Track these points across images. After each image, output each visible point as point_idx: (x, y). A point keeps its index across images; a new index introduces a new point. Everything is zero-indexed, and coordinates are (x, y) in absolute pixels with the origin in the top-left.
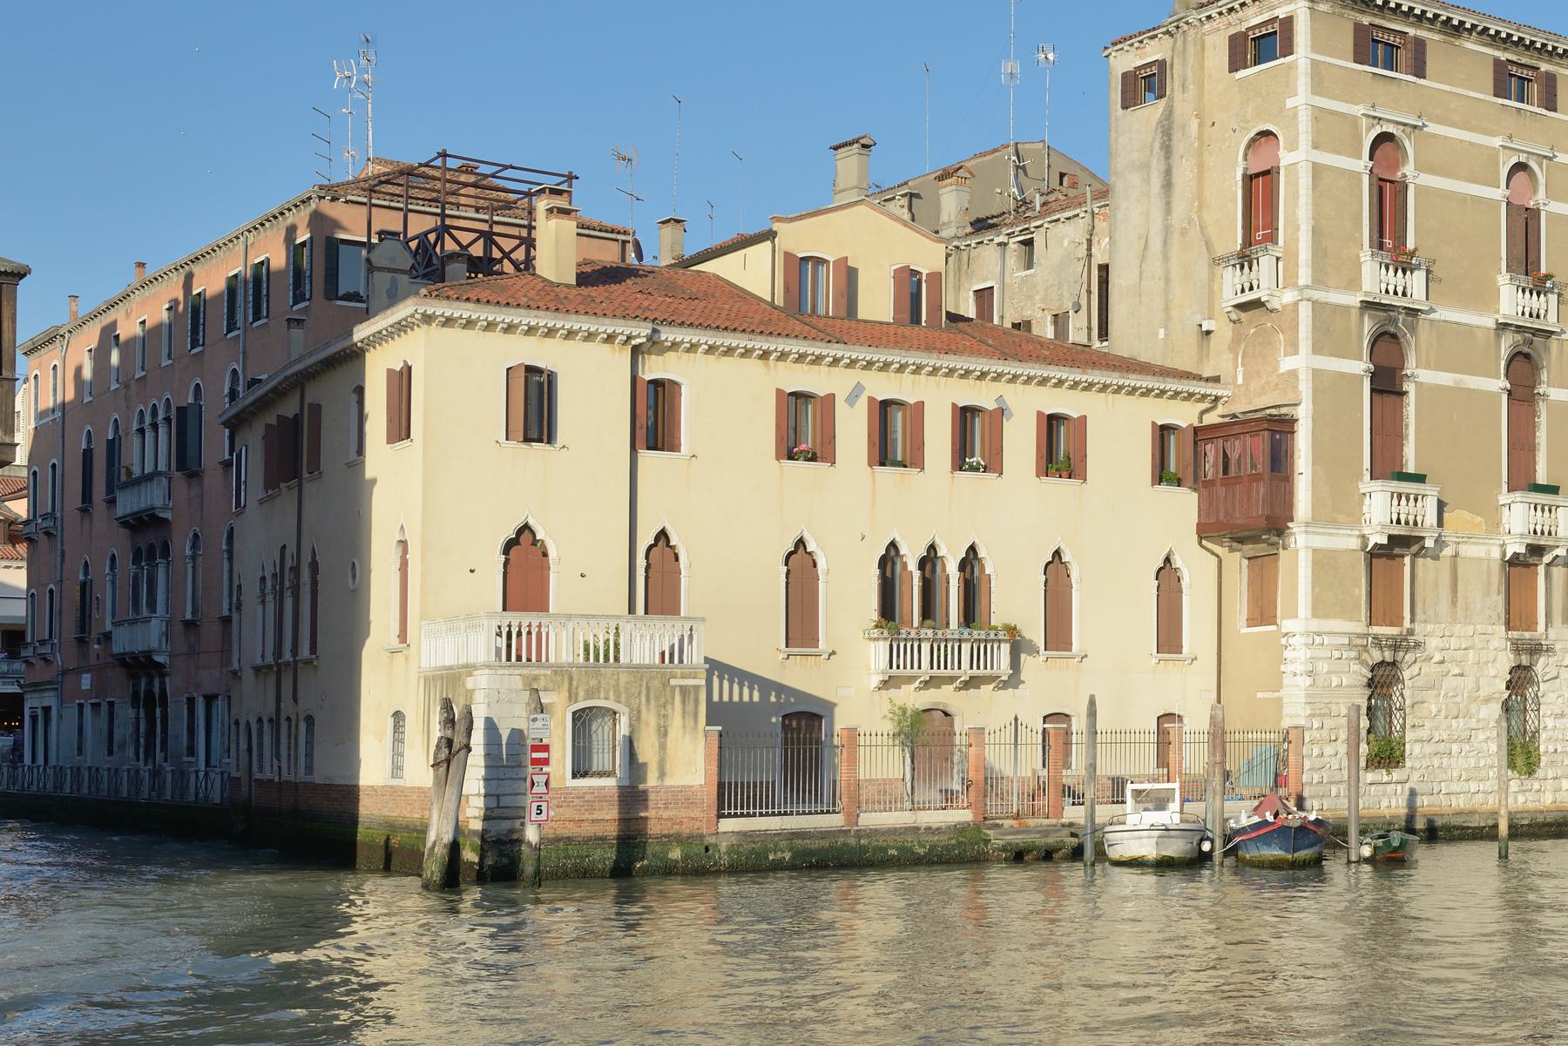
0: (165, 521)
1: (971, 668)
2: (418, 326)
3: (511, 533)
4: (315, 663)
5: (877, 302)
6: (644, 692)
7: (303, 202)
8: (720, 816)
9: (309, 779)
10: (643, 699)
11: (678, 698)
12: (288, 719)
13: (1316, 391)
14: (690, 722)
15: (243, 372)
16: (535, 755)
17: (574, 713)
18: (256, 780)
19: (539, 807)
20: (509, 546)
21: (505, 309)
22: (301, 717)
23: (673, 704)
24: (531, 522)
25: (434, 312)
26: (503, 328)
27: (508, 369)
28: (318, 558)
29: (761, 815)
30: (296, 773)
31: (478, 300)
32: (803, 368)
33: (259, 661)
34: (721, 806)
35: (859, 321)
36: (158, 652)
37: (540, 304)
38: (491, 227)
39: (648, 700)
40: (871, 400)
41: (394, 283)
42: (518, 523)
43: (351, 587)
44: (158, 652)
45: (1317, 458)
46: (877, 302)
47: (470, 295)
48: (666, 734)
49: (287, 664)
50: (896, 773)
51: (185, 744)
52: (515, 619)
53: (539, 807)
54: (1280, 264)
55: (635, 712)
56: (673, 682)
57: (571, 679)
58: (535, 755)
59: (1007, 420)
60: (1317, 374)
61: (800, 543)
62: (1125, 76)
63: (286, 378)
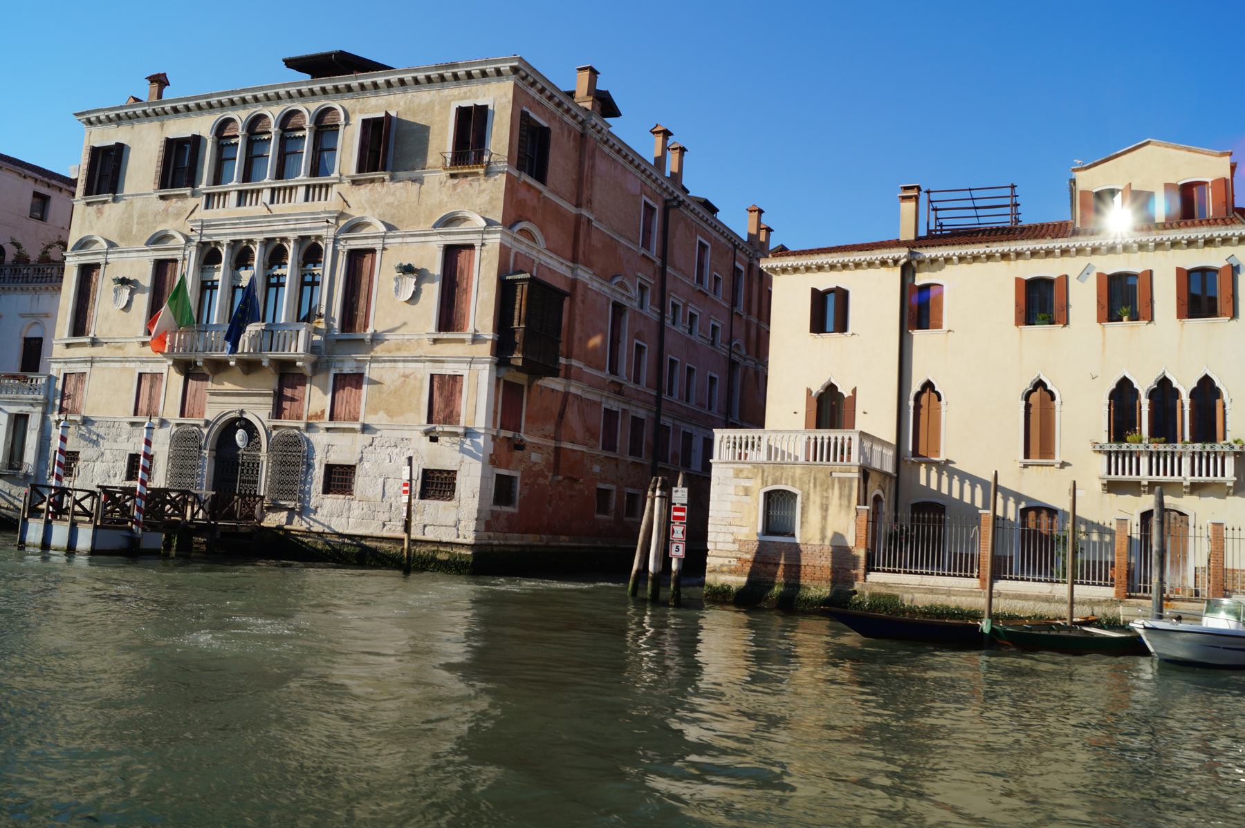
1: (1151, 474)
6: (812, 481)
10: (812, 485)
14: (845, 502)
16: (676, 514)
17: (765, 493)
19: (677, 547)
23: (833, 489)
29: (905, 572)
32: (834, 274)
39: (815, 486)
40: (1100, 275)
53: (677, 547)
57: (763, 471)
58: (676, 514)
62: (365, 122)
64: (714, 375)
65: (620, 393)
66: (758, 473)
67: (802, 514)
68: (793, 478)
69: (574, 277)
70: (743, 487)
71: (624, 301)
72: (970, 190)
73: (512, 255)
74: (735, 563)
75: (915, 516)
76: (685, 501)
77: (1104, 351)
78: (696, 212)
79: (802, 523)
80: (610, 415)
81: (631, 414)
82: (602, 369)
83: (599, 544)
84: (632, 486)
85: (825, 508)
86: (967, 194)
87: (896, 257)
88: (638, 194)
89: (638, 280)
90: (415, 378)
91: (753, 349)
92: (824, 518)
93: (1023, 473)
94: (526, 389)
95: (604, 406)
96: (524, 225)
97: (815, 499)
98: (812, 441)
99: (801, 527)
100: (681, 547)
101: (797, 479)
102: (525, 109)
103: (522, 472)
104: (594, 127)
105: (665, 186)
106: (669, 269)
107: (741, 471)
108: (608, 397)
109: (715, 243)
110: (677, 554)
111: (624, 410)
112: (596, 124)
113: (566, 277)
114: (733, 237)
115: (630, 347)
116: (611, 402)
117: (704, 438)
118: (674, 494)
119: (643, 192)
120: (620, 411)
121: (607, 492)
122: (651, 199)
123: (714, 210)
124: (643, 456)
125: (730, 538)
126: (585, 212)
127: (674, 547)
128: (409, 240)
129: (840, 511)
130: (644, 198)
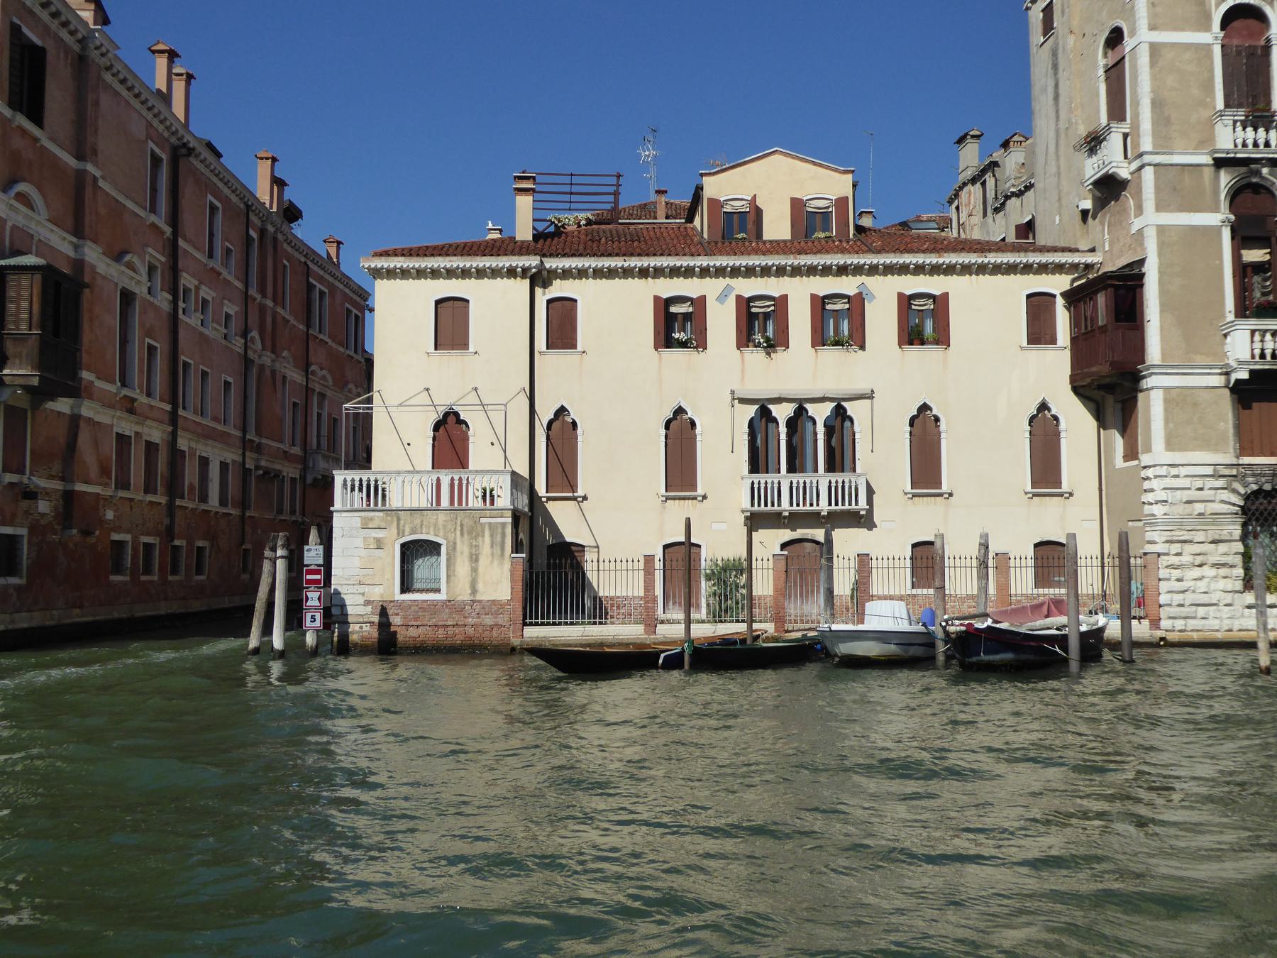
5: (777, 226)
6: (459, 528)
8: (525, 624)
10: (458, 533)
11: (487, 533)
13: (1162, 246)
14: (497, 550)
20: (437, 427)
23: (483, 536)
27: (438, 302)
29: (566, 624)
34: (525, 618)
35: (765, 242)
39: (462, 534)
40: (739, 298)
42: (674, 406)
45: (1164, 308)
46: (777, 226)
48: (477, 560)
50: (1024, 588)
52: (760, 478)
53: (312, 617)
54: (1129, 139)
55: (451, 543)
56: (483, 520)
57: (399, 519)
59: (869, 302)
60: (1161, 229)
61: (1043, 407)
64: (230, 379)
65: (131, 411)
66: (392, 522)
67: (448, 567)
68: (435, 525)
69: (78, 257)
70: (374, 538)
71: (133, 287)
72: (572, 175)
73: (8, 229)
74: (368, 629)
75: (552, 561)
77: (743, 378)
78: (207, 163)
79: (448, 577)
80: (122, 440)
81: (145, 437)
82: (113, 382)
83: (116, 615)
84: (148, 534)
85: (474, 559)
86: (567, 180)
87: (527, 265)
88: (144, 139)
89: (147, 257)
91: (269, 343)
92: (474, 570)
93: (665, 508)
94: (29, 414)
95: (115, 430)
96: (22, 187)
97: (463, 548)
98: (456, 483)
99: (448, 582)
100: (318, 616)
101: (441, 527)
102: (16, 21)
103: (28, 527)
104: (97, 48)
105: (174, 129)
106: (181, 243)
107: (372, 519)
108: (120, 418)
109: (226, 201)
110: (313, 625)
111: (137, 433)
112: (102, 45)
113: (68, 257)
114: (247, 195)
115: (141, 348)
116: (123, 424)
117: (221, 462)
118: (306, 553)
119: (149, 137)
120: (133, 435)
121: (120, 544)
122: (157, 146)
123: (219, 155)
124: (159, 492)
125: (361, 600)
126: (90, 167)
127: (309, 616)
129: (492, 562)
130: (151, 145)
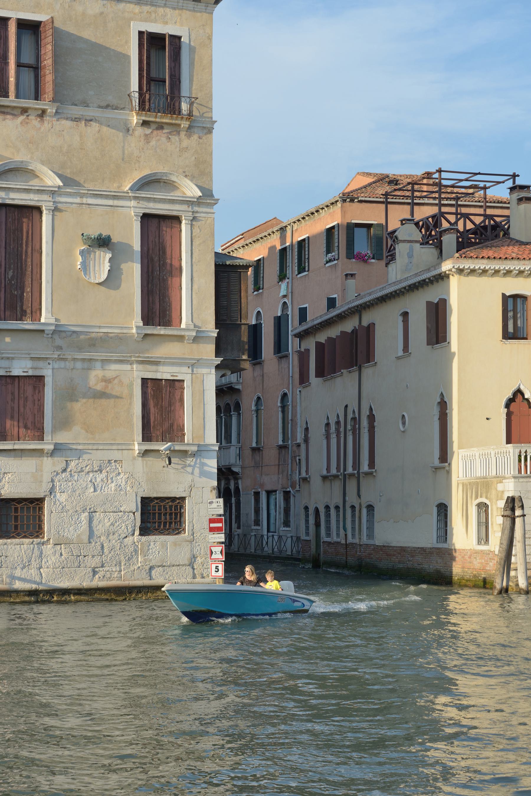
0: (238, 391)
2: (453, 275)
3: (510, 395)
4: (374, 474)
7: (332, 204)
9: (371, 542)
12: (353, 507)
15: (292, 304)
18: (323, 542)
19: (217, 567)
20: (509, 403)
21: (505, 262)
22: (364, 506)
24: (522, 388)
25: (464, 267)
26: (503, 273)
28: (374, 412)
30: (360, 539)
31: (489, 258)
33: (325, 473)
36: (235, 465)
37: (525, 256)
38: (485, 210)
41: (411, 249)
42: (514, 388)
43: (402, 429)
44: (235, 465)
47: (484, 255)
49: (351, 475)
51: (253, 518)
53: (217, 567)
58: (220, 525)
63: (349, 309)
76: (221, 512)
90: (121, 383)
128: (91, 201)
